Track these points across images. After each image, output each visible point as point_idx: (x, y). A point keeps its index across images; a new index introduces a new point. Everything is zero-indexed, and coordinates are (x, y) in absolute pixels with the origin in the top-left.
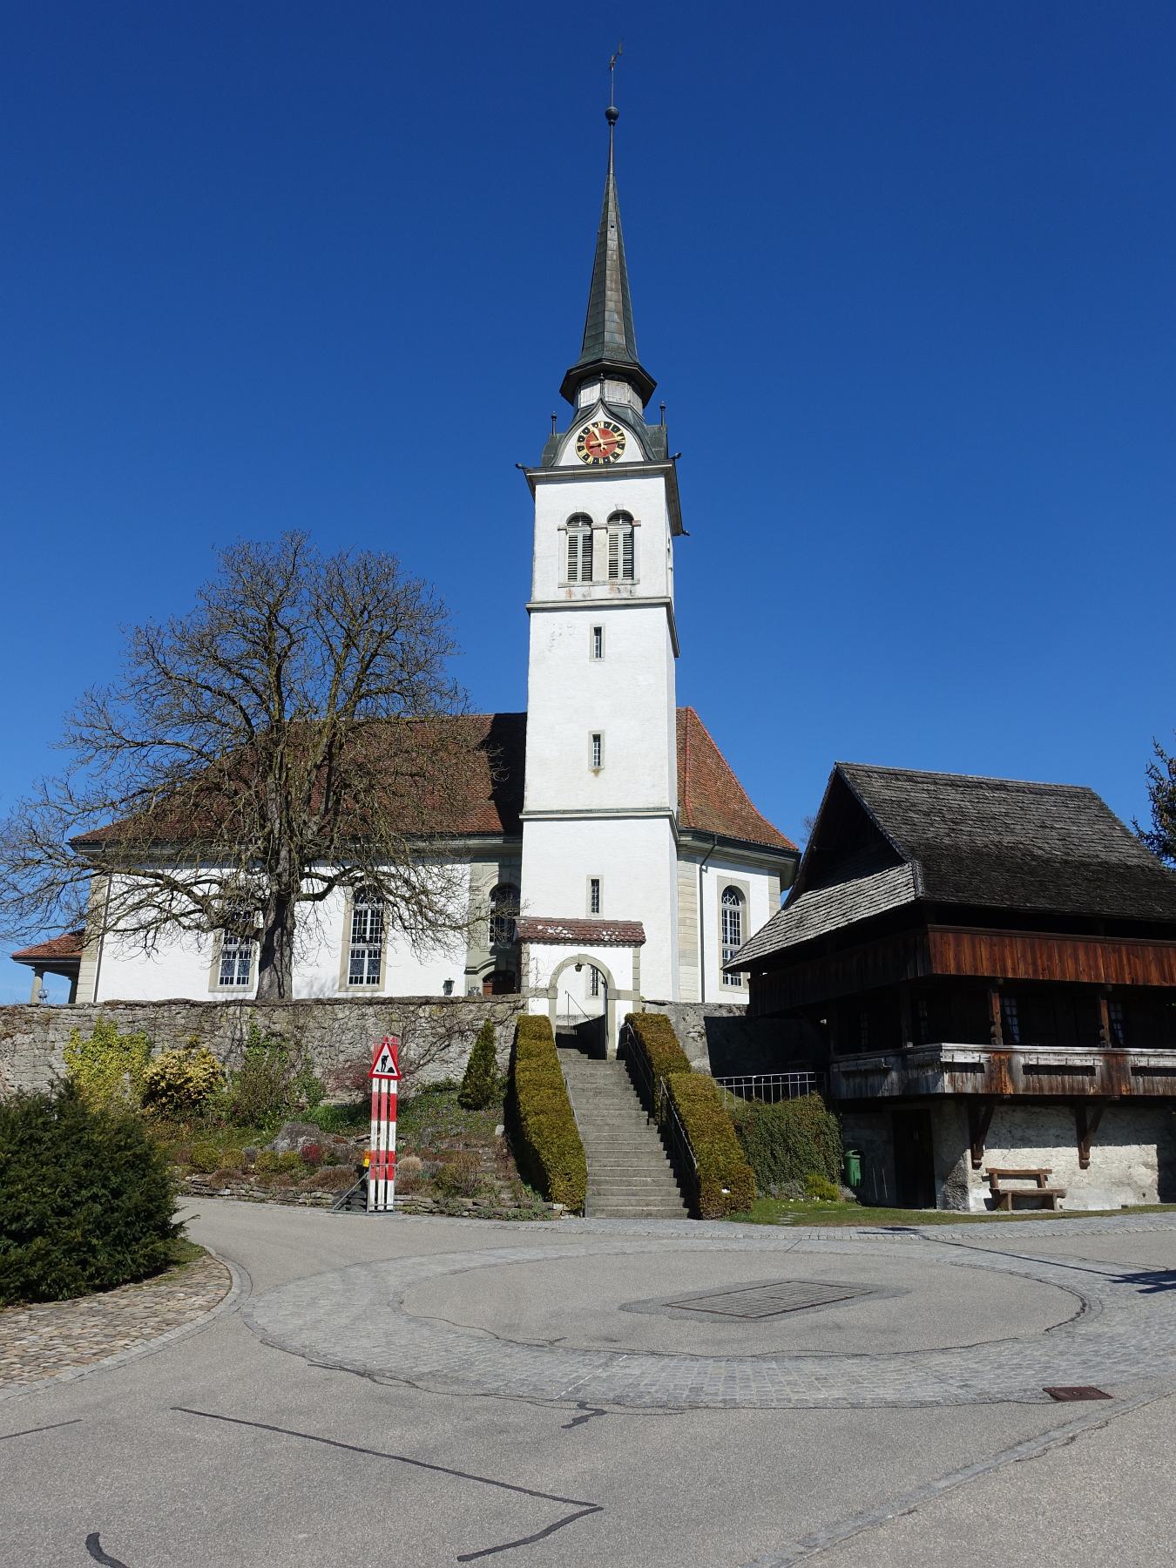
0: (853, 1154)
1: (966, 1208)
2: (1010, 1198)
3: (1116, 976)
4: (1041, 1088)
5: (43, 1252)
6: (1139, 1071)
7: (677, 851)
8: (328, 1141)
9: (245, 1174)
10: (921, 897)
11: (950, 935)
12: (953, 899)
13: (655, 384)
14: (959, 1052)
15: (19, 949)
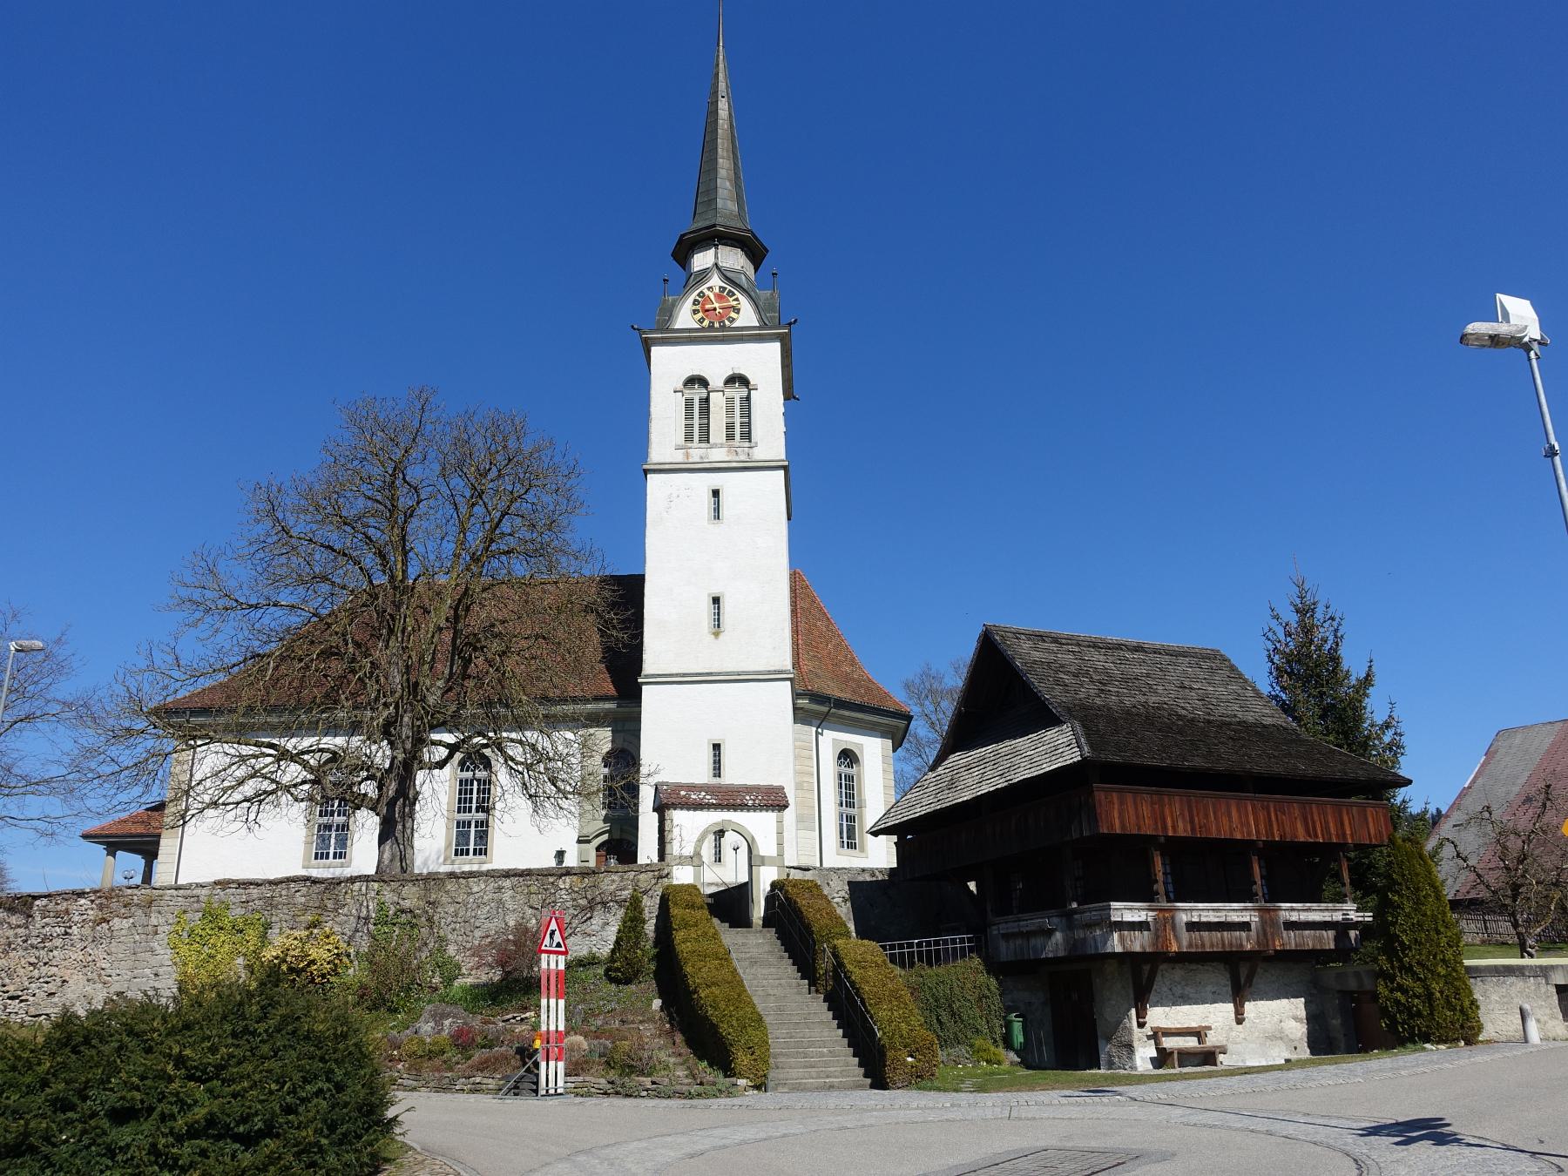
0: (1016, 1017)
1: (1133, 1068)
2: (1176, 1056)
3: (1266, 831)
4: (1203, 945)
5: (277, 1155)
6: (1291, 925)
7: (794, 714)
8: (476, 1022)
9: (390, 1061)
10: (1088, 757)
11: (1114, 794)
12: (1117, 759)
13: (767, 251)
14: (1127, 911)
15: (93, 825)
